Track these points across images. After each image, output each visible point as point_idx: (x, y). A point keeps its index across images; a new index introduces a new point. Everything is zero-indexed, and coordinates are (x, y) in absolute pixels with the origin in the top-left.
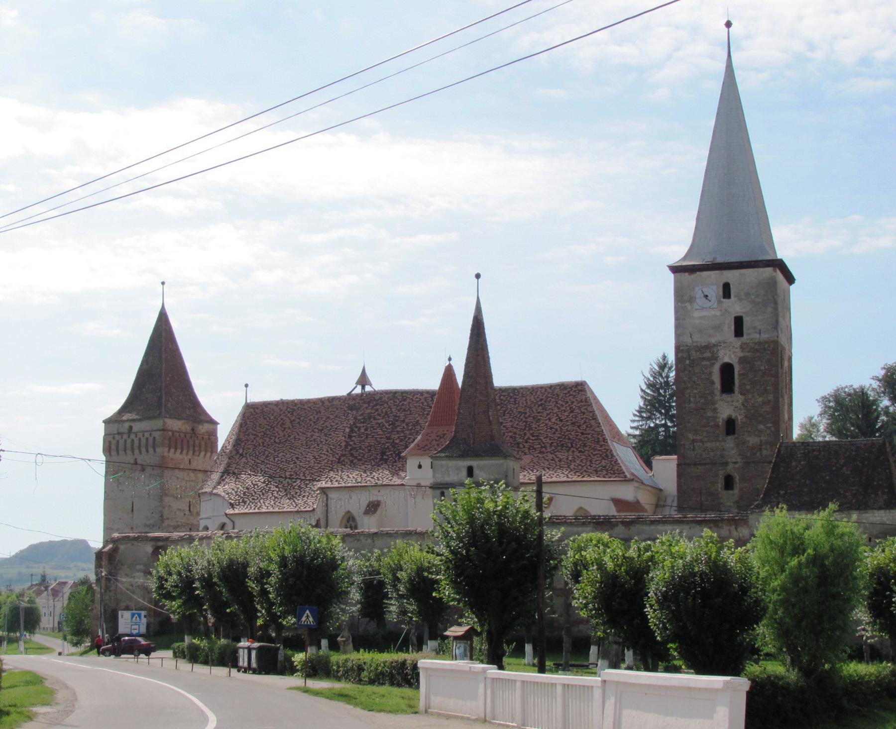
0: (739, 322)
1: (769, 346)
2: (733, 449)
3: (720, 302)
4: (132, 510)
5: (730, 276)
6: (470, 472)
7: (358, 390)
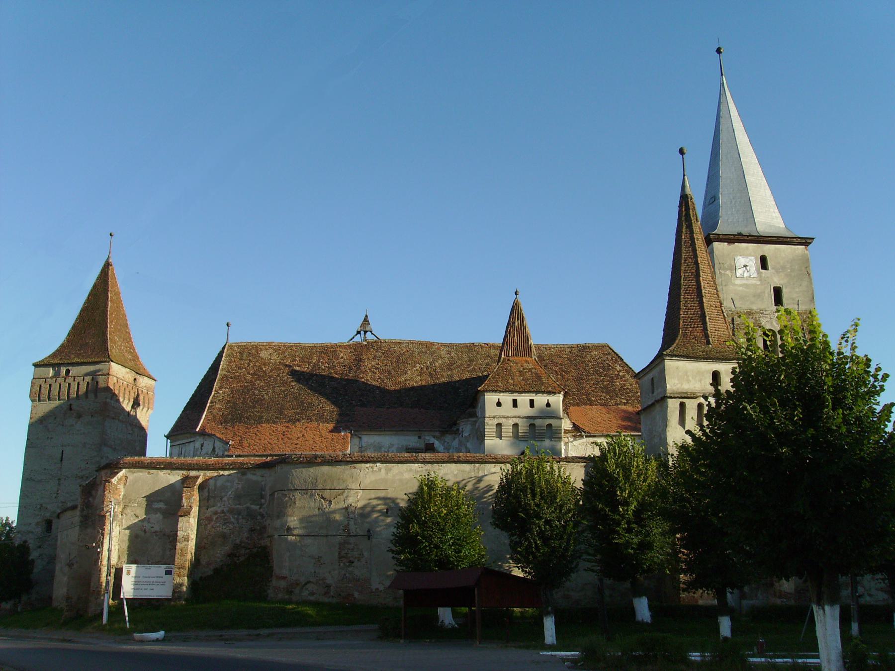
3: (758, 273)
4: (62, 460)
5: (768, 249)
7: (358, 339)
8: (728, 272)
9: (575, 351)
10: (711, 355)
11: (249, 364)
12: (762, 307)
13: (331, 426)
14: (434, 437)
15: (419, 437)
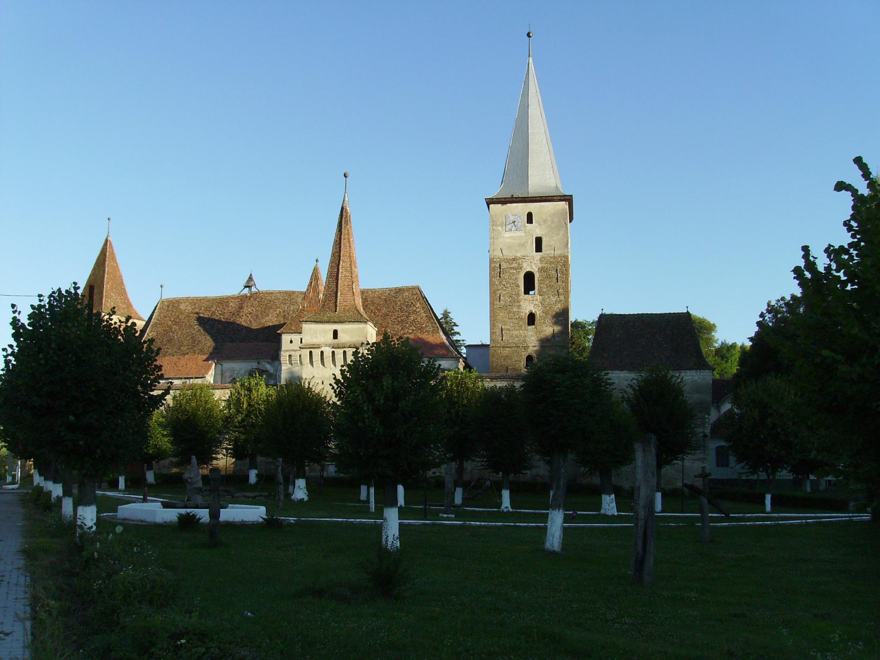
0: (539, 242)
1: (561, 260)
2: (532, 336)
6: (335, 334)
8: (499, 228)
9: (392, 293)
10: (342, 319)
11: (171, 314)
12: (524, 255)
13: (205, 357)
14: (268, 363)
15: (258, 363)
